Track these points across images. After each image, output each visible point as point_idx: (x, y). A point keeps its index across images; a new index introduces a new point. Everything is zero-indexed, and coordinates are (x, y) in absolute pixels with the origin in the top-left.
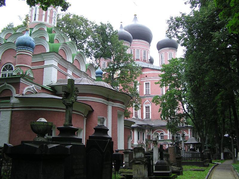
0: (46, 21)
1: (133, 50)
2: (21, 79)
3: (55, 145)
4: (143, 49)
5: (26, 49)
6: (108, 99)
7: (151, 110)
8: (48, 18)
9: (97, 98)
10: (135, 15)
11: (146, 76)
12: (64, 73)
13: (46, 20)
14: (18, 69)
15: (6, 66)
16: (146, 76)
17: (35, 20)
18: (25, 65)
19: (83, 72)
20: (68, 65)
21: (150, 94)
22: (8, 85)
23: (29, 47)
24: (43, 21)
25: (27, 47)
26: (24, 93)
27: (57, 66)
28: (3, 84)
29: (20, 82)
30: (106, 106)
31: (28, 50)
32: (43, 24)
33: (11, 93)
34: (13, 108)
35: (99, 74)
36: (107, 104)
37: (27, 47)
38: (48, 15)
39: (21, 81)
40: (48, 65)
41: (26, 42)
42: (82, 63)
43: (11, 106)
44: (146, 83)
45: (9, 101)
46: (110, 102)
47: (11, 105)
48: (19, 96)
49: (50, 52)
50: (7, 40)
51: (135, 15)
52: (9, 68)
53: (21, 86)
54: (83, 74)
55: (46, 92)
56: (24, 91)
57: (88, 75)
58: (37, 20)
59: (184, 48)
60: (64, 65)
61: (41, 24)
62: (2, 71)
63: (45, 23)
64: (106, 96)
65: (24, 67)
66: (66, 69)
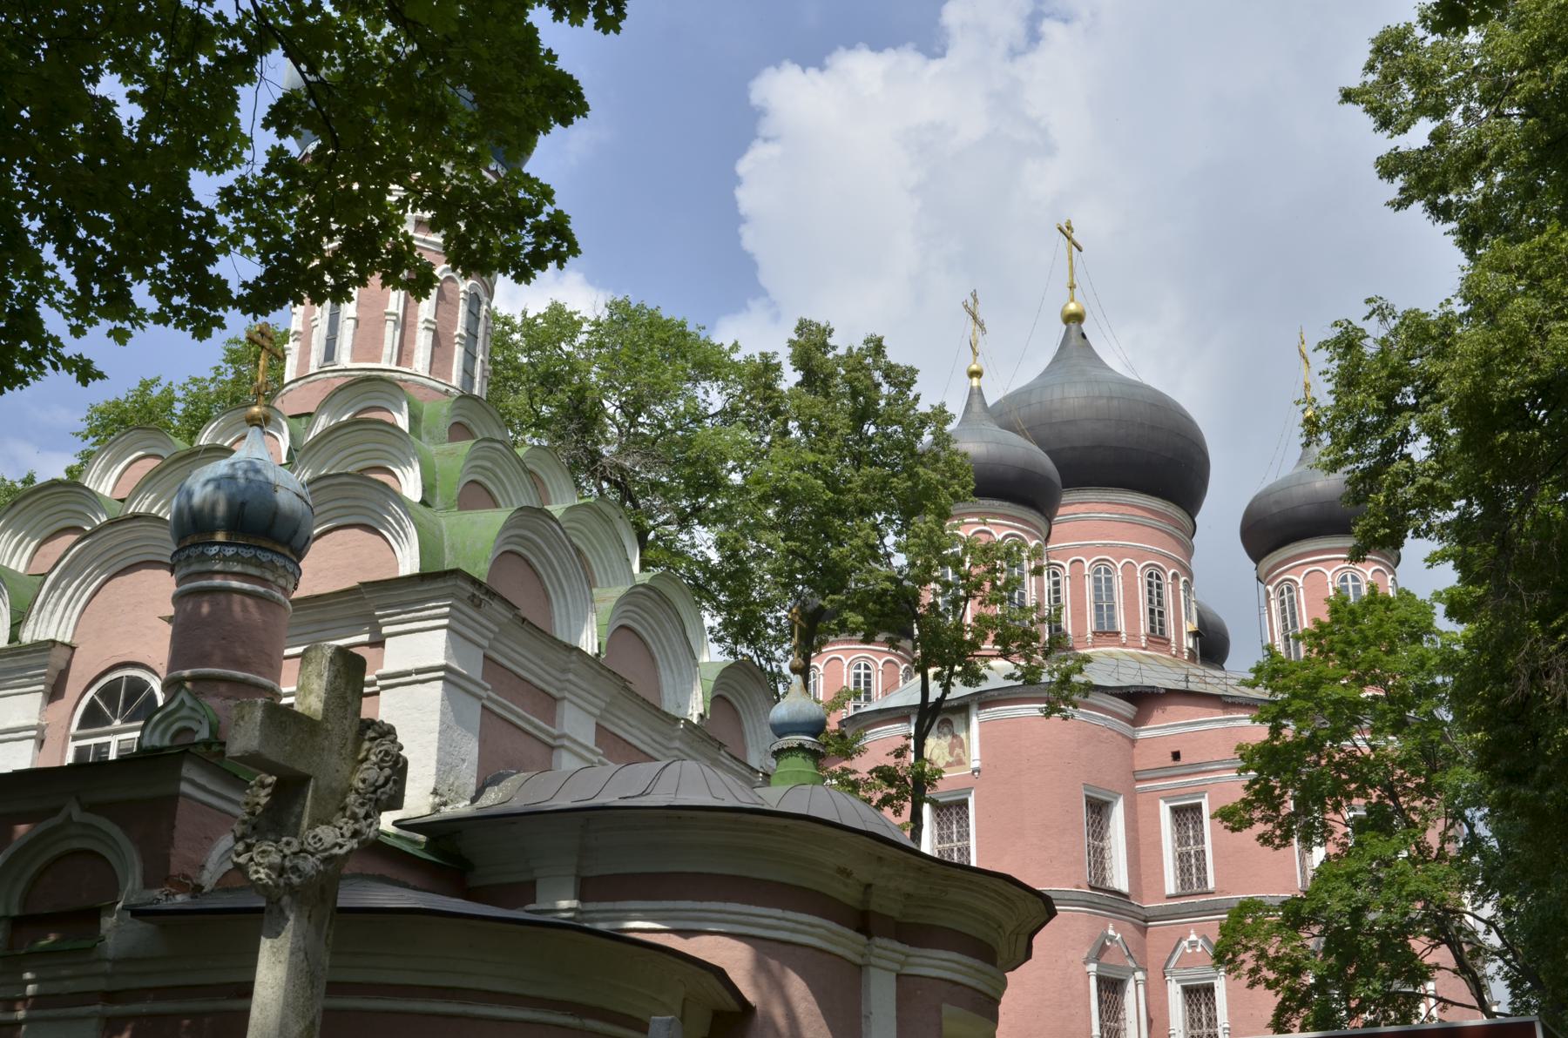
0: (410, 363)
1: (1067, 566)
2: (188, 771)
3: (44, 943)
4: (1089, 551)
5: (247, 553)
6: (864, 922)
7: (1229, 1014)
8: (422, 342)
9: (778, 912)
10: (1066, 231)
11: (1176, 756)
12: (537, 727)
13: (404, 354)
14: (182, 703)
15: (109, 693)
16: (1176, 756)
17: (330, 353)
18: (240, 674)
19: (677, 720)
20: (564, 671)
21: (1211, 885)
22: (91, 818)
23: (287, 543)
24: (387, 362)
25: (252, 542)
26: (208, 879)
27: (477, 676)
28: (55, 812)
29: (175, 797)
30: (859, 970)
31: (260, 565)
32: (390, 382)
33: (113, 887)
34: (109, 997)
35: (797, 733)
36: (859, 960)
37: (252, 542)
38: (421, 319)
39: (185, 788)
40: (408, 673)
41: (243, 504)
42: (669, 640)
43: (102, 985)
44: (1176, 811)
45: (86, 944)
46: (884, 942)
47: (105, 975)
48: (165, 905)
49: (421, 578)
50: (122, 500)
51: (1075, 319)
52: (128, 703)
53: (185, 823)
54: (680, 739)
55: (387, 871)
56: (210, 866)
57: (721, 745)
58: (344, 359)
59: (931, 437)
60: (510, 660)
61: (368, 379)
62: (74, 729)
63: (402, 373)
64: (848, 894)
65: (223, 688)
66: (548, 703)
